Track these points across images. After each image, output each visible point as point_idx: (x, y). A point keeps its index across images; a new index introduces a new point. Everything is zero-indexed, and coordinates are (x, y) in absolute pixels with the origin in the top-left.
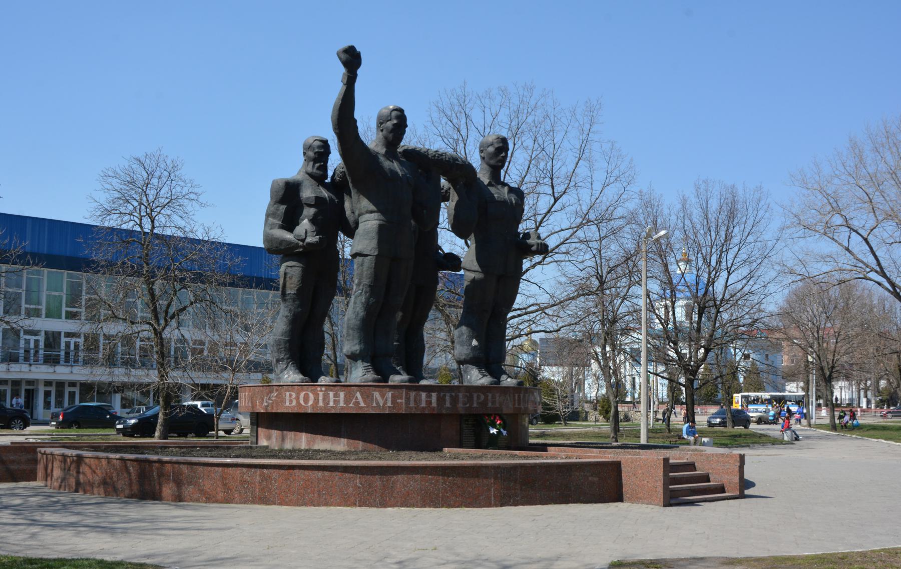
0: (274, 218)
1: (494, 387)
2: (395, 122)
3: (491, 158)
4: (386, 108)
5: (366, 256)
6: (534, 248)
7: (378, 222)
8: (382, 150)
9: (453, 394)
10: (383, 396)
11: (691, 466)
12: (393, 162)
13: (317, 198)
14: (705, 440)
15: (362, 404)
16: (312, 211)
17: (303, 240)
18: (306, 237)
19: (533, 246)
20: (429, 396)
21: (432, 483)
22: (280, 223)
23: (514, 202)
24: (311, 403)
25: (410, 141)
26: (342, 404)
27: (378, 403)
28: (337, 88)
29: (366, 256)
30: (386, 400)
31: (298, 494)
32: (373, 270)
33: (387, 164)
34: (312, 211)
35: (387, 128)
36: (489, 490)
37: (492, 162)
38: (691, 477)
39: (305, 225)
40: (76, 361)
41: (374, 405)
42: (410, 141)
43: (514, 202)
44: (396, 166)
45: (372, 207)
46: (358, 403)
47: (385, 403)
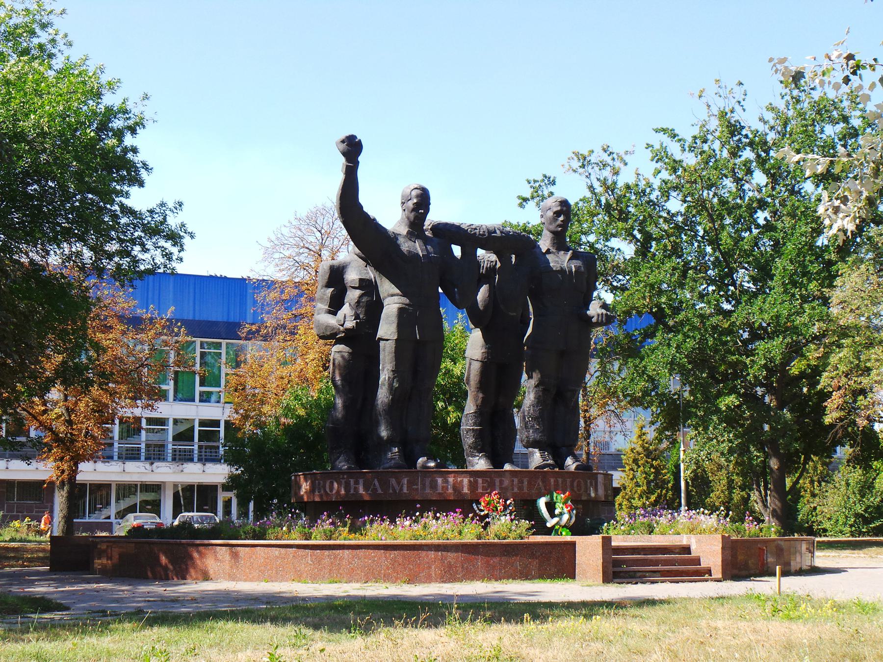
0: (321, 303)
1: (538, 472)
2: (415, 201)
3: (551, 224)
4: (407, 188)
5: (387, 340)
6: (594, 320)
7: (397, 306)
8: (403, 230)
9: (472, 479)
10: (399, 483)
11: (687, 550)
12: (415, 242)
13: (361, 280)
14: (149, 507)
15: (380, 491)
16: (358, 293)
17: (342, 325)
18: (344, 322)
19: (593, 317)
20: (521, 482)
21: (374, 561)
22: (327, 307)
23: (574, 270)
24: (334, 492)
25: (436, 215)
26: (525, 490)
27: (394, 490)
28: (338, 178)
29: (387, 340)
30: (402, 486)
31: (260, 571)
32: (394, 354)
33: (406, 246)
34: (358, 293)
35: (408, 208)
36: (430, 567)
37: (552, 227)
38: (670, 560)
39: (346, 310)
40: (138, 454)
41: (391, 491)
42: (436, 215)
43: (574, 270)
44: (418, 247)
45: (397, 291)
46: (376, 490)
47: (401, 489)
